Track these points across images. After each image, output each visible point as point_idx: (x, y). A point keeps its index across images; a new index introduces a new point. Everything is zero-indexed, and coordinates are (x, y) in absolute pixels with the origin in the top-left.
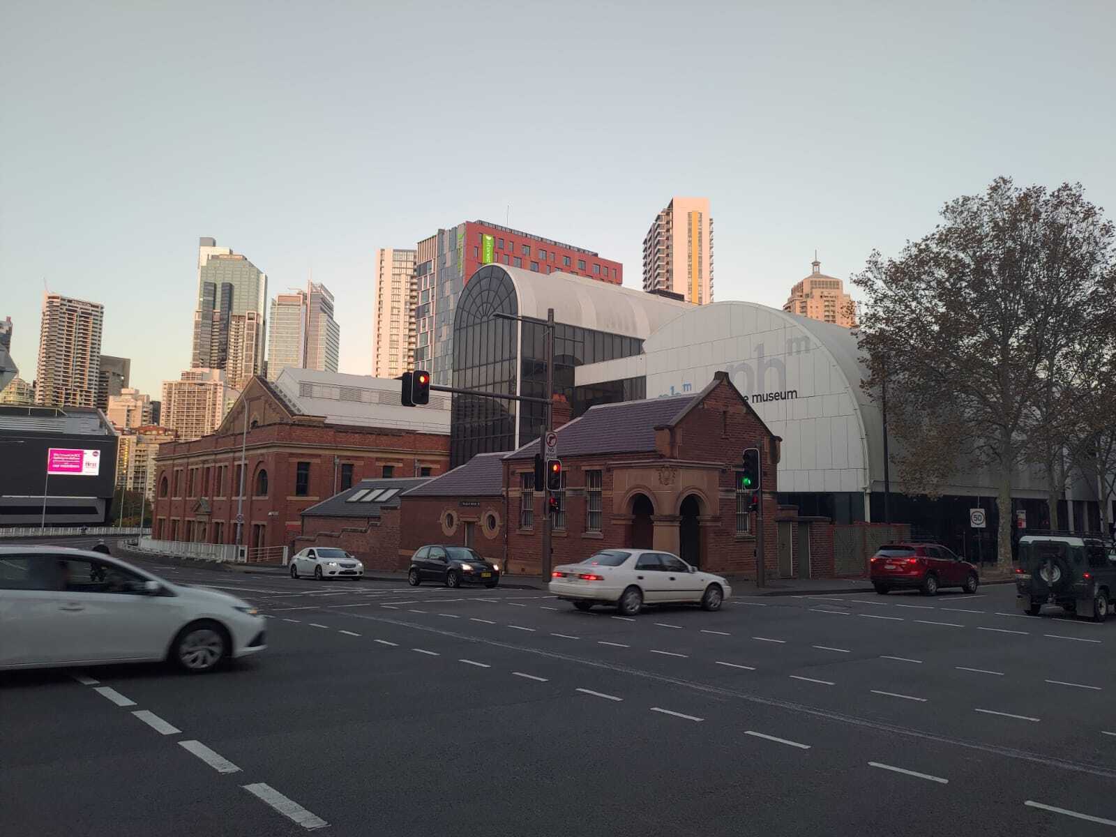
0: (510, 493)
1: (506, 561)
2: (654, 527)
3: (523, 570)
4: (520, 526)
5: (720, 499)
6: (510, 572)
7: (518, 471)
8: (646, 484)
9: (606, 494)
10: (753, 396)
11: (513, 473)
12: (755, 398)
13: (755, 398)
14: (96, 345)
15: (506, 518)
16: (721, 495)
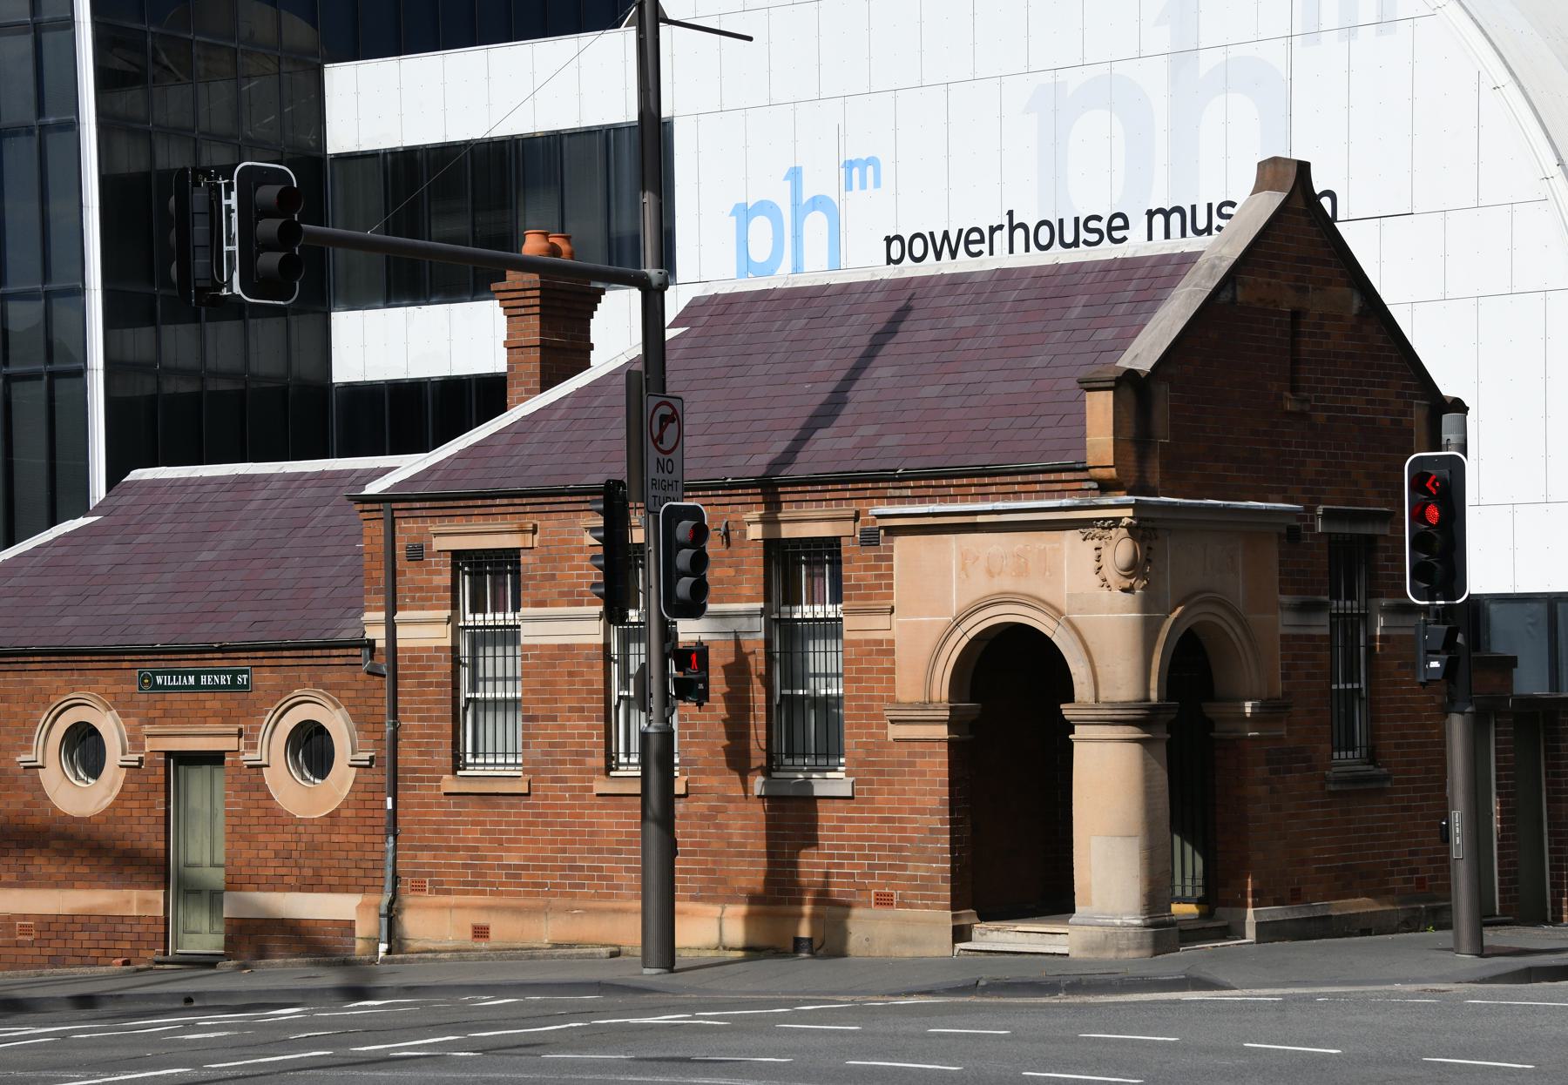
0: (401, 632)
1: (392, 902)
2: (1077, 746)
3: (480, 932)
4: (457, 763)
5: (1283, 637)
6: (416, 945)
7: (440, 544)
8: (1044, 593)
9: (856, 627)
10: (1151, 214)
11: (417, 553)
12: (1159, 220)
13: (1159, 220)
14: (511, 269)
15: (389, 729)
16: (1286, 623)
